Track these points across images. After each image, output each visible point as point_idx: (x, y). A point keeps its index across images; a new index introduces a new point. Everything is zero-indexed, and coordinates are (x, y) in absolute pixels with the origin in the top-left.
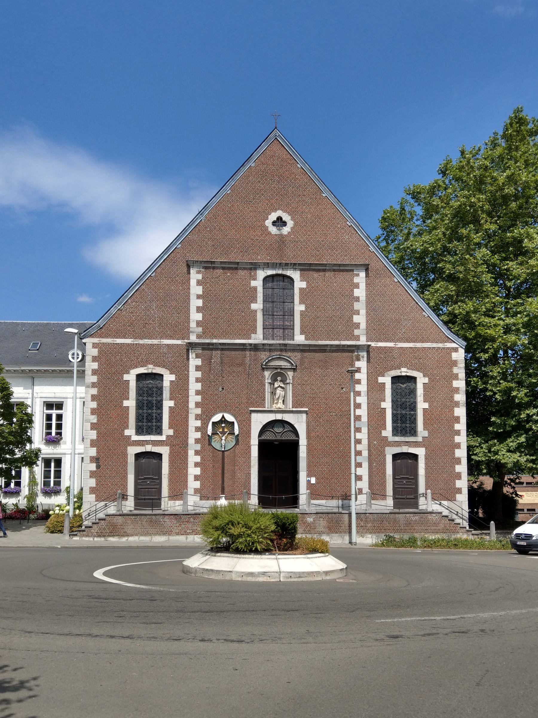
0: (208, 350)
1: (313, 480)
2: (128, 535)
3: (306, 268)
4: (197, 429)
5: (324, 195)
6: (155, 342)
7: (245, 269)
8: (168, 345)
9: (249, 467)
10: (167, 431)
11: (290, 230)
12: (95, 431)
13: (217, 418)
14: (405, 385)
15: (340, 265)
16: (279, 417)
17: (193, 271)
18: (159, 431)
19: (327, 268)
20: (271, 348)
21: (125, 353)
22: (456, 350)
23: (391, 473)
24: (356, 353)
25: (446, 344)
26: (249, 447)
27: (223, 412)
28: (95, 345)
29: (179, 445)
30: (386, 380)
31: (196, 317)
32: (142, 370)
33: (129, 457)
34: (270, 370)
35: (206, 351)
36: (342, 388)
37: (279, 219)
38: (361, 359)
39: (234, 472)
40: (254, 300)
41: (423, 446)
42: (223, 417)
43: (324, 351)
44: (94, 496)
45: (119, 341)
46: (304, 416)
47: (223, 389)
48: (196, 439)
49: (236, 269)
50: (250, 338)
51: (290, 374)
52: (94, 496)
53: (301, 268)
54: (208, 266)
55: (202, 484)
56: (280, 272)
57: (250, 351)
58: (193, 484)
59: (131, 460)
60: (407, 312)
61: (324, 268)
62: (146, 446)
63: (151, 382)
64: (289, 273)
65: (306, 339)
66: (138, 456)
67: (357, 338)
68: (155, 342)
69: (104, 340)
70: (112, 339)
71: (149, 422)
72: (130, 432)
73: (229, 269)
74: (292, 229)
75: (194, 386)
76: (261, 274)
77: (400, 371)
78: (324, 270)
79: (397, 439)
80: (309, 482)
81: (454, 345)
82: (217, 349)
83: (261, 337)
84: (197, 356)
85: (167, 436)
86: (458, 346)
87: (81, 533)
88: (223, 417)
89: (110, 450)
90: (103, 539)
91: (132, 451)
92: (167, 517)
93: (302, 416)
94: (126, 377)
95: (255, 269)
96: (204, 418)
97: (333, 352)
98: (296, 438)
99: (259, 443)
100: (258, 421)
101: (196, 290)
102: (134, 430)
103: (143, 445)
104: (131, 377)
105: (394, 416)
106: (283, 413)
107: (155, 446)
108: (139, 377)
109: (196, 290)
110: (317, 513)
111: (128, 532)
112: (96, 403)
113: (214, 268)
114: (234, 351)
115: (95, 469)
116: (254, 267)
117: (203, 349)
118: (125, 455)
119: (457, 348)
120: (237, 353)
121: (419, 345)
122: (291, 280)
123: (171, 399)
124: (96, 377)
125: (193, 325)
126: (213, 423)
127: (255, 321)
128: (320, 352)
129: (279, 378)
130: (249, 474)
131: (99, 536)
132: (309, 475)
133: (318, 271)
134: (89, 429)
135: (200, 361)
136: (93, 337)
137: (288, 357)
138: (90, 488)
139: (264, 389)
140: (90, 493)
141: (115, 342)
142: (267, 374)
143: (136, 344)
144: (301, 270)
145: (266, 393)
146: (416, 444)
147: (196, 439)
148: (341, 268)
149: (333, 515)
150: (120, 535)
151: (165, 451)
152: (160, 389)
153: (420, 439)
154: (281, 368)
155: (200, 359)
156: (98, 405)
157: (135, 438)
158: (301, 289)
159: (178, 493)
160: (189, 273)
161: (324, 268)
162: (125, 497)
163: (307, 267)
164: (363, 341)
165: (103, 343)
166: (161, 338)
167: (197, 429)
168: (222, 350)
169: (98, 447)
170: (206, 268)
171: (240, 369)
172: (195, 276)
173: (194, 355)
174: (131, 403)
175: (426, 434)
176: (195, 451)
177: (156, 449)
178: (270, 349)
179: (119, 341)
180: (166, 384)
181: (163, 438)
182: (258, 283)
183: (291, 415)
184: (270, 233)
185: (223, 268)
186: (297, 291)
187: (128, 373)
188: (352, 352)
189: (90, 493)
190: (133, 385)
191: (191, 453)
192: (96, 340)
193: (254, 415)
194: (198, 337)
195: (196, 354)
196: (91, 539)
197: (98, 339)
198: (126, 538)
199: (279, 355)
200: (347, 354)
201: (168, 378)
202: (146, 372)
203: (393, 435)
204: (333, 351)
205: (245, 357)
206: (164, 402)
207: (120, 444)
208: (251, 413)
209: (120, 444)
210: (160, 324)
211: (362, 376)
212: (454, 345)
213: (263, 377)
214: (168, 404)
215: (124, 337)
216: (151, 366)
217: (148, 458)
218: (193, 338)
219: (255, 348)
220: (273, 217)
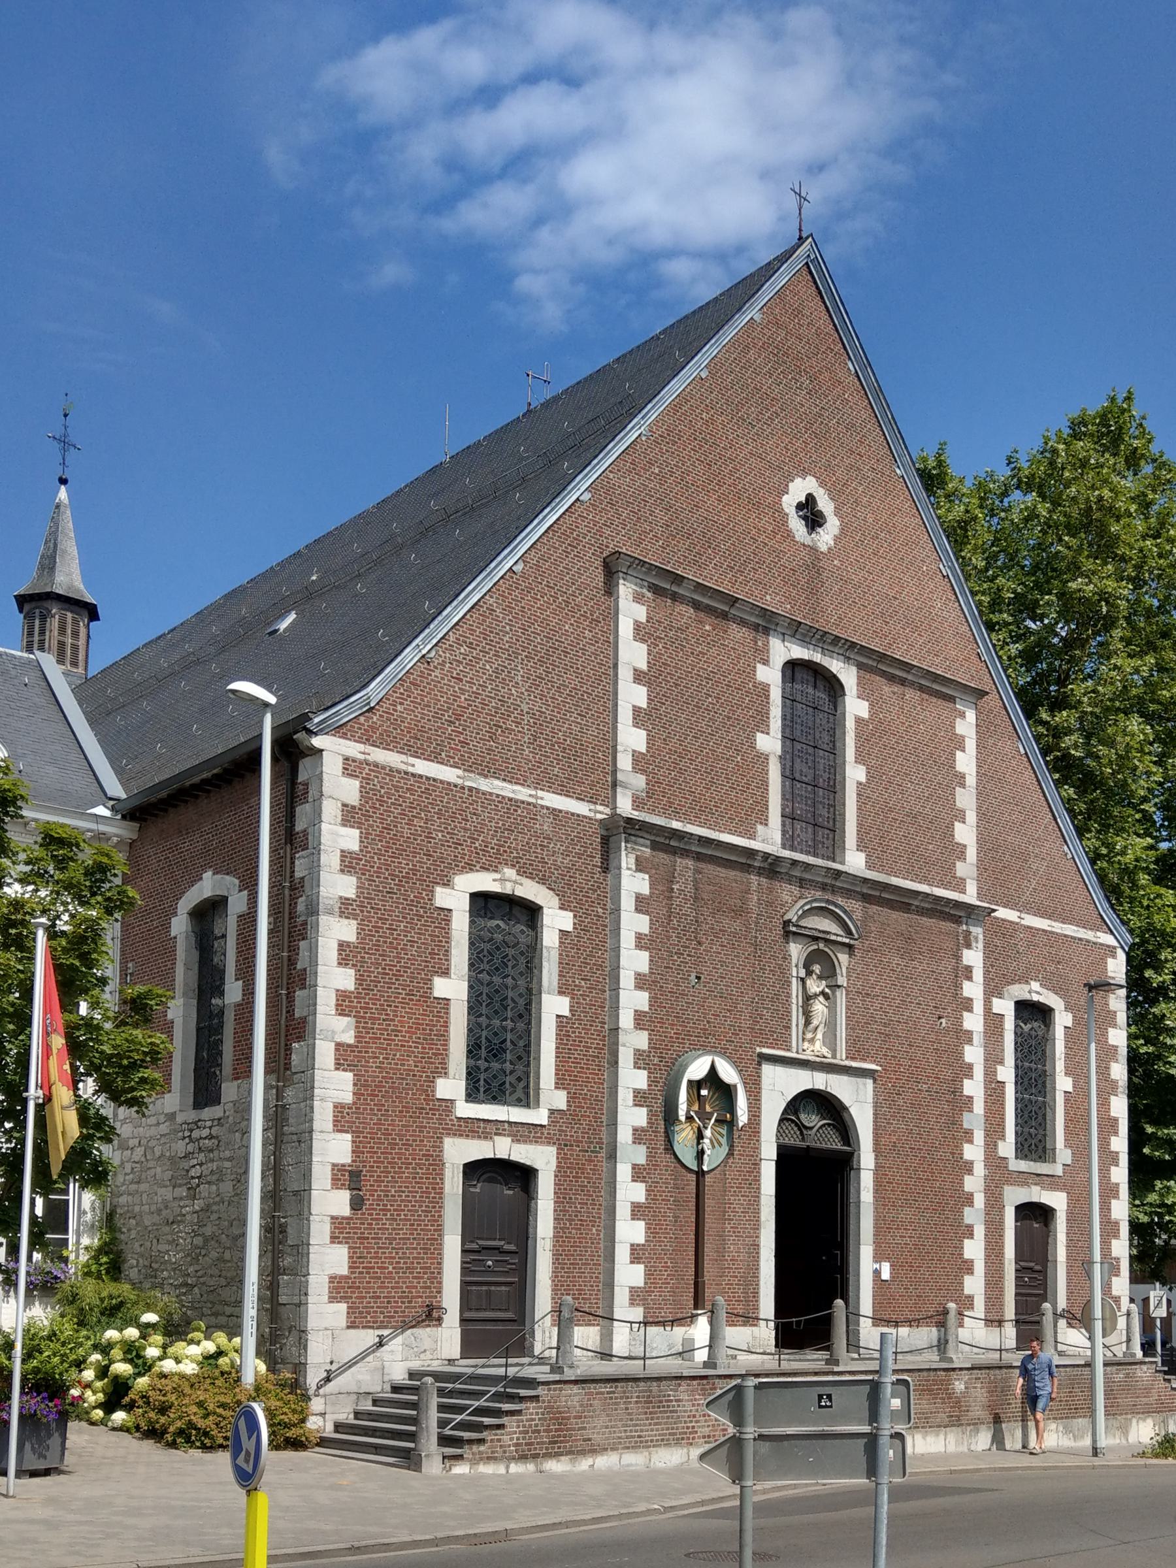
0: (666, 852)
1: (886, 1275)
2: (594, 1451)
3: (877, 665)
4: (640, 1098)
5: (898, 471)
6: (523, 793)
7: (743, 622)
8: (555, 812)
9: (757, 1227)
10: (1064, 1155)
11: (832, 543)
12: (350, 1075)
13: (698, 1069)
14: (1029, 1026)
15: (936, 678)
16: (819, 1081)
17: (625, 589)
18: (527, 1099)
19: (910, 677)
20: (807, 876)
21: (439, 813)
22: (1112, 951)
23: (1013, 1256)
24: (964, 927)
25: (1099, 934)
26: (757, 1165)
27: (716, 1053)
28: (351, 767)
29: (585, 1138)
30: (1005, 1007)
31: (632, 739)
32: (486, 882)
33: (448, 1173)
34: (800, 939)
35: (662, 855)
36: (940, 1018)
37: (810, 500)
38: (974, 944)
39: (722, 1237)
40: (762, 724)
41: (549, 1141)
42: (713, 1069)
43: (905, 907)
44: (343, 1307)
45: (422, 767)
46: (869, 1082)
47: (698, 978)
48: (635, 1130)
49: (724, 616)
50: (752, 837)
51: (843, 958)
52: (343, 1307)
53: (865, 661)
54: (664, 585)
55: (648, 1275)
56: (817, 657)
57: (759, 874)
58: (629, 1275)
59: (453, 1184)
60: (1039, 839)
61: (904, 675)
62: (496, 1138)
63: (501, 923)
64: (836, 666)
65: (869, 866)
66: (473, 1170)
67: (960, 886)
68: (523, 793)
69: (380, 756)
70: (403, 758)
71: (500, 1065)
72: (451, 1087)
73: (710, 610)
74: (837, 539)
75: (634, 961)
76: (782, 650)
77: (1026, 987)
78: (903, 682)
79: (1024, 1166)
80: (877, 1273)
81: (1109, 940)
82: (685, 853)
83: (777, 837)
84: (640, 866)
85: (552, 1112)
86: (1116, 944)
87: (475, 1448)
88: (713, 1069)
89: (393, 1145)
90: (531, 1467)
91: (460, 1152)
92: (684, 1386)
93: (865, 1084)
94: (443, 897)
95: (766, 631)
96: (663, 1065)
97: (922, 915)
98: (839, 1146)
99: (778, 1155)
100: (781, 1085)
101: (633, 654)
102: (464, 1083)
103: (486, 1136)
104: (454, 898)
105: (473, 1031)
106: (828, 1072)
107: (518, 1141)
108: (482, 902)
109: (633, 654)
110: (972, 1368)
111: (597, 1438)
112: (352, 972)
113: (675, 597)
114: (725, 867)
115: (346, 1211)
116: (766, 623)
117: (655, 846)
118: (437, 1165)
119: (1115, 948)
120: (732, 873)
121: (1058, 927)
122: (834, 687)
123: (561, 993)
124: (353, 880)
125: (625, 762)
126: (690, 1082)
127: (765, 784)
128: (899, 909)
129: (817, 968)
130: (757, 1246)
131: (523, 1458)
132: (878, 1258)
133: (892, 678)
134: (332, 1067)
135: (647, 883)
136: (344, 736)
137: (845, 912)
138: (332, 1279)
139: (789, 995)
140: (332, 1299)
141: (411, 769)
142: (796, 951)
143: (471, 789)
144: (860, 666)
145: (794, 1007)
146: (1050, 1182)
147: (635, 1130)
148: (936, 686)
149: (997, 1372)
150: (576, 1453)
151: (542, 1159)
152: (533, 950)
153: (1058, 1170)
154: (827, 941)
155: (647, 877)
156: (360, 980)
157: (466, 1110)
158: (859, 720)
159: (587, 1301)
160: (610, 590)
161: (904, 675)
162: (435, 1314)
163: (870, 662)
164: (970, 896)
165: (376, 765)
166: (537, 785)
167: (640, 1098)
168: (699, 857)
169: (356, 1133)
170: (656, 590)
171: (737, 925)
172: (631, 610)
173: (632, 860)
174: (453, 988)
175: (560, 1100)
176: (634, 1166)
177: (521, 1153)
178: (801, 880)
179: (422, 767)
180: (550, 939)
181: (540, 1116)
182: (770, 675)
183: (845, 1079)
184: (789, 535)
185: (697, 606)
186: (850, 724)
187: (447, 884)
188: (957, 920)
189: (332, 1299)
190: (460, 924)
191: (624, 1171)
192: (354, 749)
193: (767, 1069)
194: (638, 803)
195: (637, 859)
196: (501, 1469)
197: (361, 747)
198: (590, 1461)
199: (828, 901)
200: (949, 924)
201: (556, 921)
202: (496, 888)
203: (1017, 1158)
204: (922, 912)
205: (748, 892)
206: (543, 995)
207: (422, 1128)
208: (759, 1064)
209: (422, 1128)
210: (535, 738)
211: (973, 989)
212: (1109, 940)
213: (787, 957)
214: (554, 1006)
215: (434, 757)
216: (510, 873)
217: (490, 1180)
218: (625, 806)
219: (745, 860)
220: (800, 488)
